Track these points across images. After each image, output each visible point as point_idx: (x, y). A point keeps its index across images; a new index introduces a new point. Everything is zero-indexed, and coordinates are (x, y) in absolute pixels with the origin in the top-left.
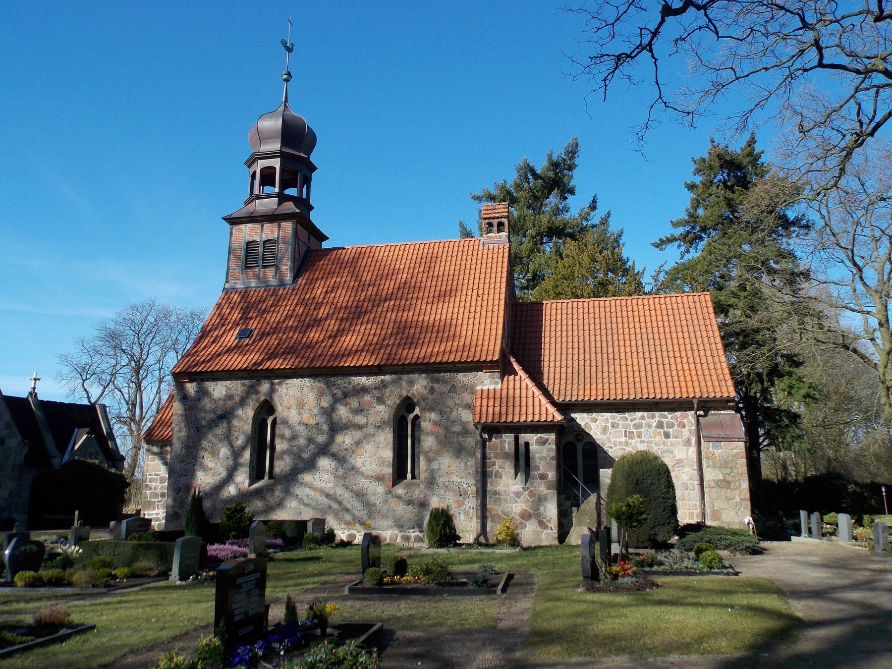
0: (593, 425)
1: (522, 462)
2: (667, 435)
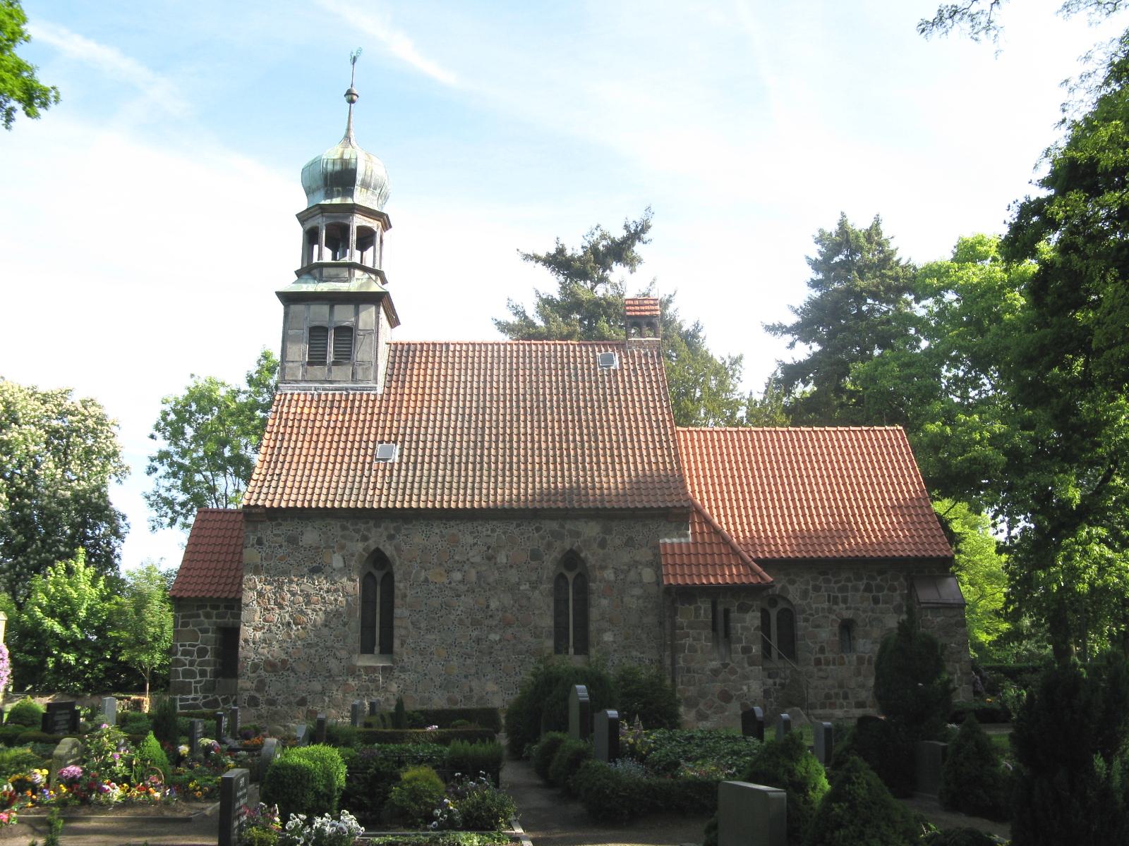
0: (791, 588)
1: (721, 633)
2: (876, 601)
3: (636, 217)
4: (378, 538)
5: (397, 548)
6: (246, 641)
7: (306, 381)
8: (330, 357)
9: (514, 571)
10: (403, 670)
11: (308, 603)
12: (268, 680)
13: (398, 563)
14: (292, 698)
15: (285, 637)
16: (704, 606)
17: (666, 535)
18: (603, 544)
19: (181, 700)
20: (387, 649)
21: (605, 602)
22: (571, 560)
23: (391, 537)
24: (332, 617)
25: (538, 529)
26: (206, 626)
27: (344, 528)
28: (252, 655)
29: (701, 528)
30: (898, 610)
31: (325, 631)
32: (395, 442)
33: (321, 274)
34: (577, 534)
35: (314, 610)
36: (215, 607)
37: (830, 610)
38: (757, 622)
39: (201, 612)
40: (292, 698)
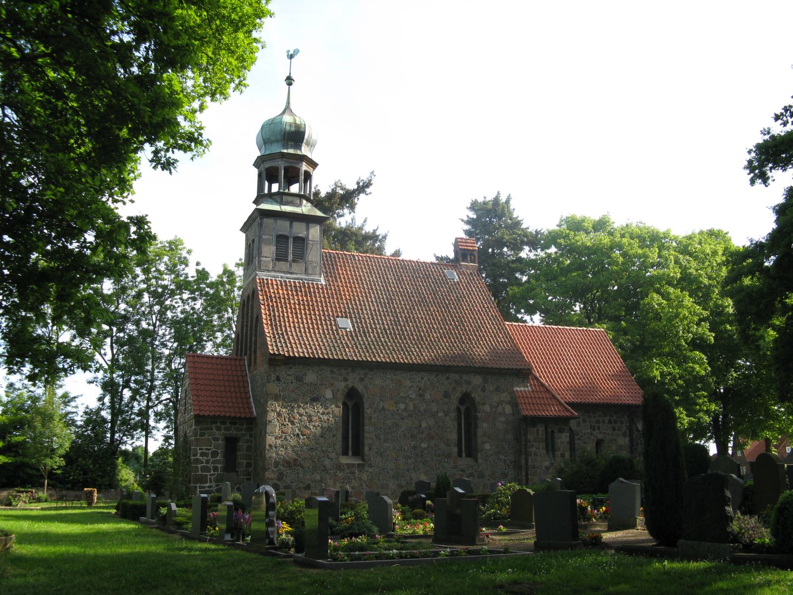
2: (614, 429)
3: (365, 177)
4: (354, 380)
5: (366, 387)
6: (270, 446)
7: (275, 271)
8: (290, 257)
9: (434, 404)
10: (370, 466)
11: (310, 421)
12: (285, 473)
13: (366, 396)
14: (301, 485)
15: (296, 444)
16: (541, 428)
17: (517, 386)
18: (483, 390)
19: (200, 487)
20: (358, 452)
21: (485, 425)
22: (466, 398)
23: (362, 380)
24: (326, 431)
25: (448, 379)
26: (217, 436)
27: (332, 372)
28: (274, 455)
29: (534, 382)
30: (624, 435)
31: (322, 440)
32: (346, 317)
33: (282, 199)
34: (469, 383)
35: (314, 426)
36: (223, 423)
37: (591, 434)
38: (568, 439)
39: (213, 426)
40: (301, 485)
